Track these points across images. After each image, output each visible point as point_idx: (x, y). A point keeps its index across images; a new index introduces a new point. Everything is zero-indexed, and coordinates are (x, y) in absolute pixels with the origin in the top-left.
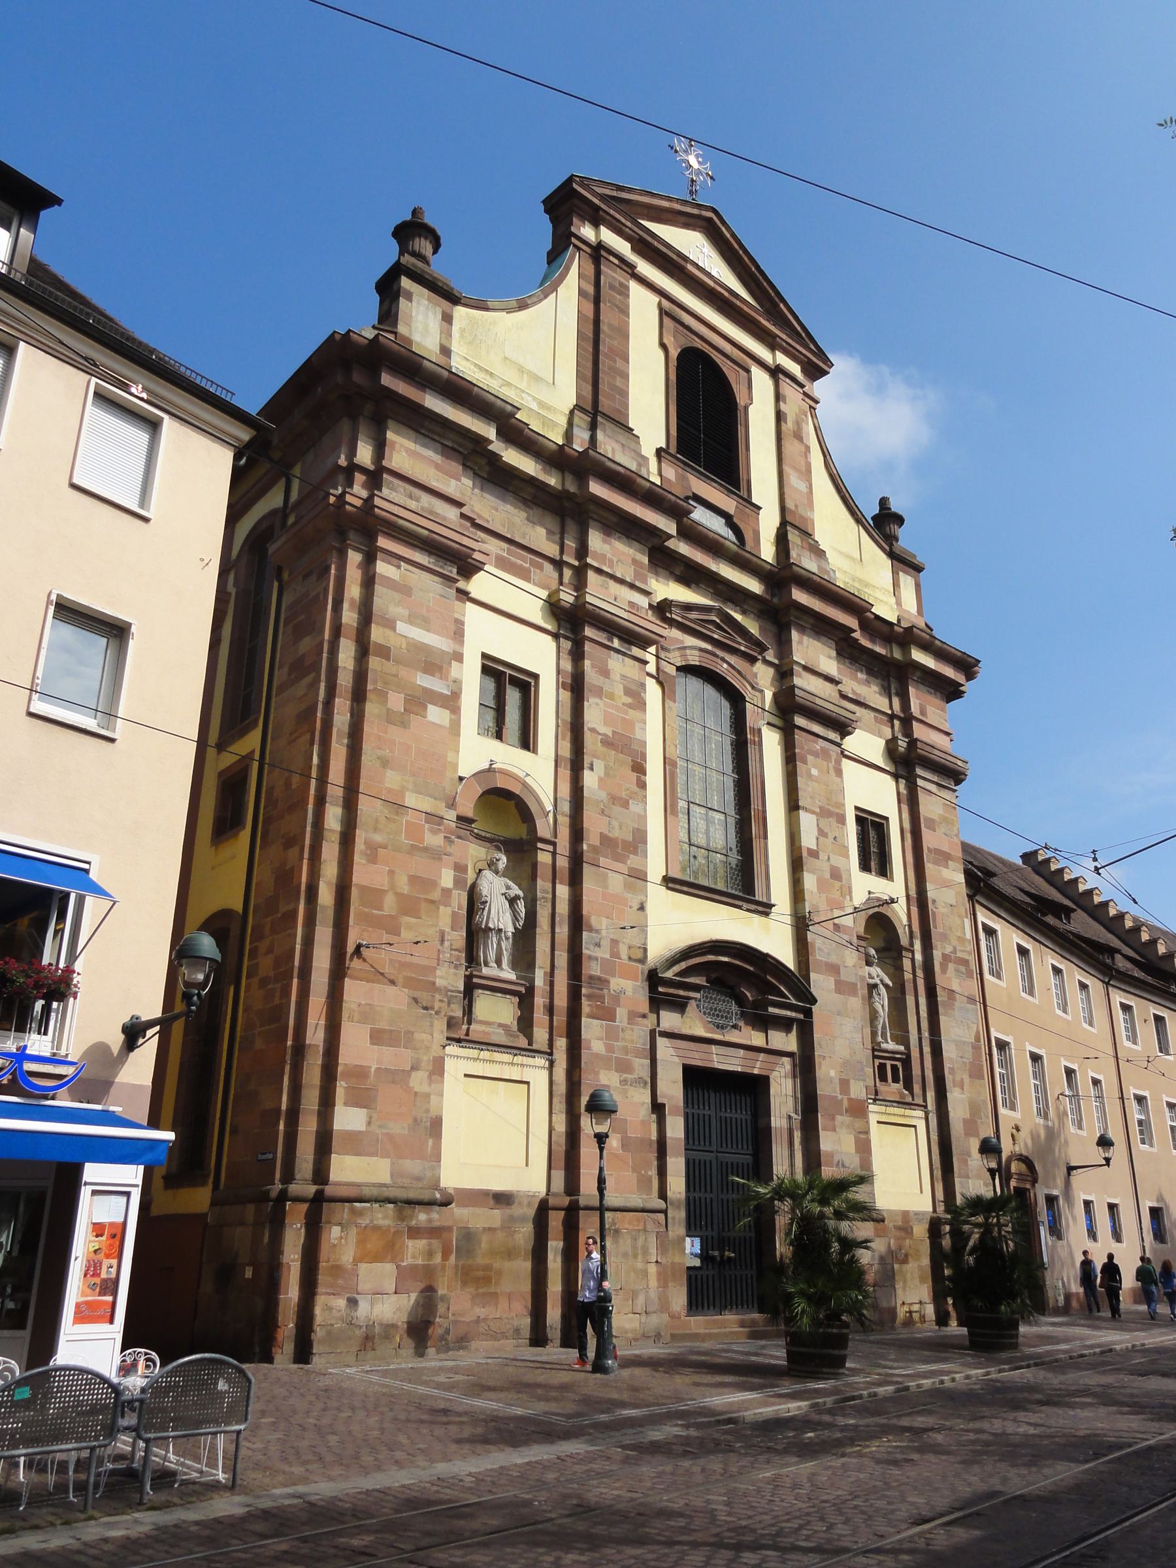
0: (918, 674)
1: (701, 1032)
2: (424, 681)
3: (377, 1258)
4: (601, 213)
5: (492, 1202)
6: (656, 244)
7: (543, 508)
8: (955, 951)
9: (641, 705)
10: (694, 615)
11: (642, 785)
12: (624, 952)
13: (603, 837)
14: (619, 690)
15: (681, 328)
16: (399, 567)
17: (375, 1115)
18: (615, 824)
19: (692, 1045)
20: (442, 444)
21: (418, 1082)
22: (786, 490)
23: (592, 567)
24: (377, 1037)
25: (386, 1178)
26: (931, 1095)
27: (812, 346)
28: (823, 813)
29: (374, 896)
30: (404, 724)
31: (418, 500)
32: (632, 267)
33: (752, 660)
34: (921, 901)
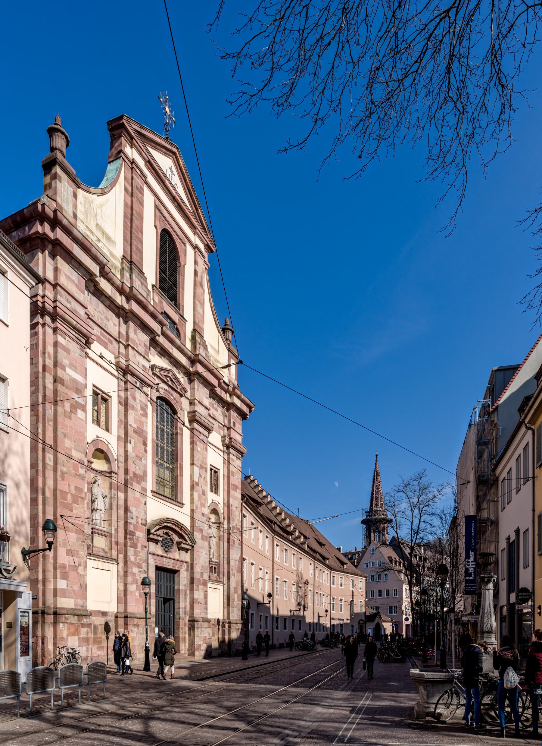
3: (73, 635)
5: (101, 615)
8: (236, 525)
9: (145, 415)
10: (163, 373)
11: (146, 451)
13: (134, 474)
14: (139, 407)
15: (162, 217)
18: (137, 467)
21: (80, 569)
22: (196, 313)
23: (131, 346)
25: (73, 606)
26: (226, 578)
28: (201, 467)
29: (65, 493)
31: (70, 303)
32: (146, 177)
33: (181, 396)
34: (228, 505)
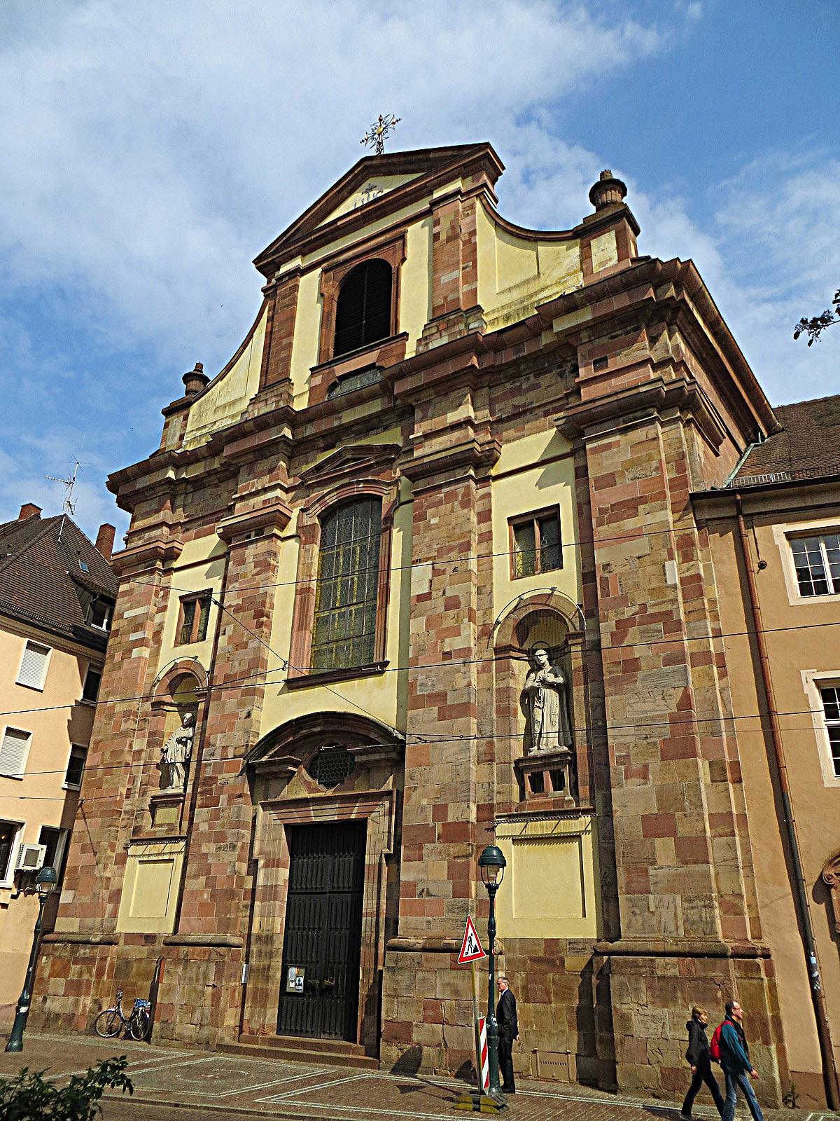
3: (58, 976)
5: (143, 941)
10: (327, 468)
25: (76, 929)
27: (358, 199)
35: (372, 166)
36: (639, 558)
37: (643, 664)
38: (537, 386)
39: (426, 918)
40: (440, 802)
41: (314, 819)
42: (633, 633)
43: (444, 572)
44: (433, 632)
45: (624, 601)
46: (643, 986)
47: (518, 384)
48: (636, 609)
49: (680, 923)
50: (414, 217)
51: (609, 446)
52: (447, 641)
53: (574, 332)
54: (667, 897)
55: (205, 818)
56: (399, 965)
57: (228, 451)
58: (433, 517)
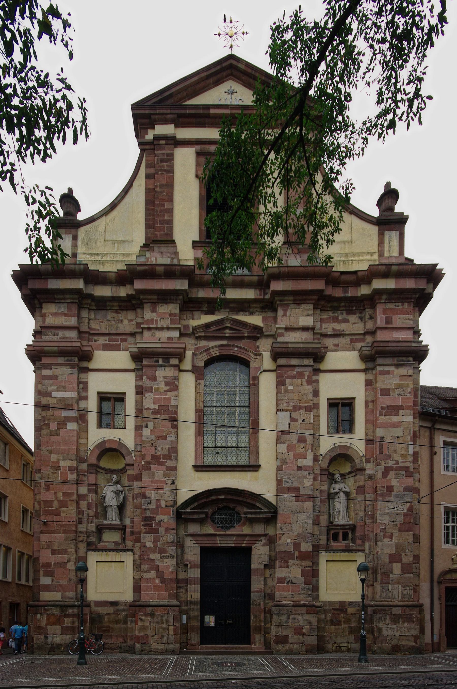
0: (384, 297)
1: (212, 531)
2: (64, 413)
3: (54, 624)
4: (153, 117)
6: (188, 111)
7: (126, 310)
10: (213, 328)
12: (163, 503)
16: (51, 369)
17: (54, 579)
19: (205, 538)
20: (67, 303)
24: (54, 552)
25: (60, 599)
30: (57, 434)
35: (236, 68)
36: (398, 437)
37: (395, 489)
38: (346, 321)
39: (291, 593)
40: (297, 541)
41: (219, 545)
42: (392, 474)
43: (296, 421)
44: (291, 454)
45: (389, 457)
46: (388, 617)
47: (336, 315)
48: (394, 462)
49: (400, 595)
50: (185, 144)
51: (388, 373)
52: (299, 460)
53: (378, 293)
54: (396, 586)
55: (150, 540)
56: (281, 612)
57: (139, 285)
58: (290, 385)
